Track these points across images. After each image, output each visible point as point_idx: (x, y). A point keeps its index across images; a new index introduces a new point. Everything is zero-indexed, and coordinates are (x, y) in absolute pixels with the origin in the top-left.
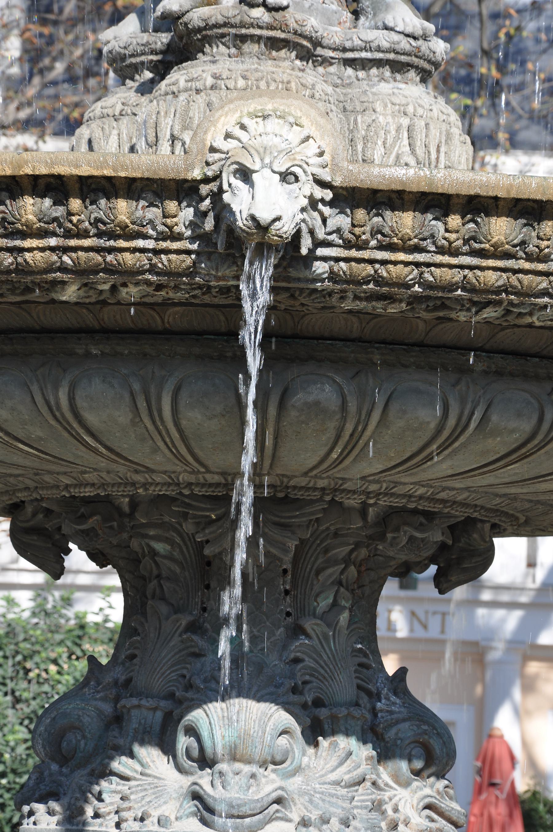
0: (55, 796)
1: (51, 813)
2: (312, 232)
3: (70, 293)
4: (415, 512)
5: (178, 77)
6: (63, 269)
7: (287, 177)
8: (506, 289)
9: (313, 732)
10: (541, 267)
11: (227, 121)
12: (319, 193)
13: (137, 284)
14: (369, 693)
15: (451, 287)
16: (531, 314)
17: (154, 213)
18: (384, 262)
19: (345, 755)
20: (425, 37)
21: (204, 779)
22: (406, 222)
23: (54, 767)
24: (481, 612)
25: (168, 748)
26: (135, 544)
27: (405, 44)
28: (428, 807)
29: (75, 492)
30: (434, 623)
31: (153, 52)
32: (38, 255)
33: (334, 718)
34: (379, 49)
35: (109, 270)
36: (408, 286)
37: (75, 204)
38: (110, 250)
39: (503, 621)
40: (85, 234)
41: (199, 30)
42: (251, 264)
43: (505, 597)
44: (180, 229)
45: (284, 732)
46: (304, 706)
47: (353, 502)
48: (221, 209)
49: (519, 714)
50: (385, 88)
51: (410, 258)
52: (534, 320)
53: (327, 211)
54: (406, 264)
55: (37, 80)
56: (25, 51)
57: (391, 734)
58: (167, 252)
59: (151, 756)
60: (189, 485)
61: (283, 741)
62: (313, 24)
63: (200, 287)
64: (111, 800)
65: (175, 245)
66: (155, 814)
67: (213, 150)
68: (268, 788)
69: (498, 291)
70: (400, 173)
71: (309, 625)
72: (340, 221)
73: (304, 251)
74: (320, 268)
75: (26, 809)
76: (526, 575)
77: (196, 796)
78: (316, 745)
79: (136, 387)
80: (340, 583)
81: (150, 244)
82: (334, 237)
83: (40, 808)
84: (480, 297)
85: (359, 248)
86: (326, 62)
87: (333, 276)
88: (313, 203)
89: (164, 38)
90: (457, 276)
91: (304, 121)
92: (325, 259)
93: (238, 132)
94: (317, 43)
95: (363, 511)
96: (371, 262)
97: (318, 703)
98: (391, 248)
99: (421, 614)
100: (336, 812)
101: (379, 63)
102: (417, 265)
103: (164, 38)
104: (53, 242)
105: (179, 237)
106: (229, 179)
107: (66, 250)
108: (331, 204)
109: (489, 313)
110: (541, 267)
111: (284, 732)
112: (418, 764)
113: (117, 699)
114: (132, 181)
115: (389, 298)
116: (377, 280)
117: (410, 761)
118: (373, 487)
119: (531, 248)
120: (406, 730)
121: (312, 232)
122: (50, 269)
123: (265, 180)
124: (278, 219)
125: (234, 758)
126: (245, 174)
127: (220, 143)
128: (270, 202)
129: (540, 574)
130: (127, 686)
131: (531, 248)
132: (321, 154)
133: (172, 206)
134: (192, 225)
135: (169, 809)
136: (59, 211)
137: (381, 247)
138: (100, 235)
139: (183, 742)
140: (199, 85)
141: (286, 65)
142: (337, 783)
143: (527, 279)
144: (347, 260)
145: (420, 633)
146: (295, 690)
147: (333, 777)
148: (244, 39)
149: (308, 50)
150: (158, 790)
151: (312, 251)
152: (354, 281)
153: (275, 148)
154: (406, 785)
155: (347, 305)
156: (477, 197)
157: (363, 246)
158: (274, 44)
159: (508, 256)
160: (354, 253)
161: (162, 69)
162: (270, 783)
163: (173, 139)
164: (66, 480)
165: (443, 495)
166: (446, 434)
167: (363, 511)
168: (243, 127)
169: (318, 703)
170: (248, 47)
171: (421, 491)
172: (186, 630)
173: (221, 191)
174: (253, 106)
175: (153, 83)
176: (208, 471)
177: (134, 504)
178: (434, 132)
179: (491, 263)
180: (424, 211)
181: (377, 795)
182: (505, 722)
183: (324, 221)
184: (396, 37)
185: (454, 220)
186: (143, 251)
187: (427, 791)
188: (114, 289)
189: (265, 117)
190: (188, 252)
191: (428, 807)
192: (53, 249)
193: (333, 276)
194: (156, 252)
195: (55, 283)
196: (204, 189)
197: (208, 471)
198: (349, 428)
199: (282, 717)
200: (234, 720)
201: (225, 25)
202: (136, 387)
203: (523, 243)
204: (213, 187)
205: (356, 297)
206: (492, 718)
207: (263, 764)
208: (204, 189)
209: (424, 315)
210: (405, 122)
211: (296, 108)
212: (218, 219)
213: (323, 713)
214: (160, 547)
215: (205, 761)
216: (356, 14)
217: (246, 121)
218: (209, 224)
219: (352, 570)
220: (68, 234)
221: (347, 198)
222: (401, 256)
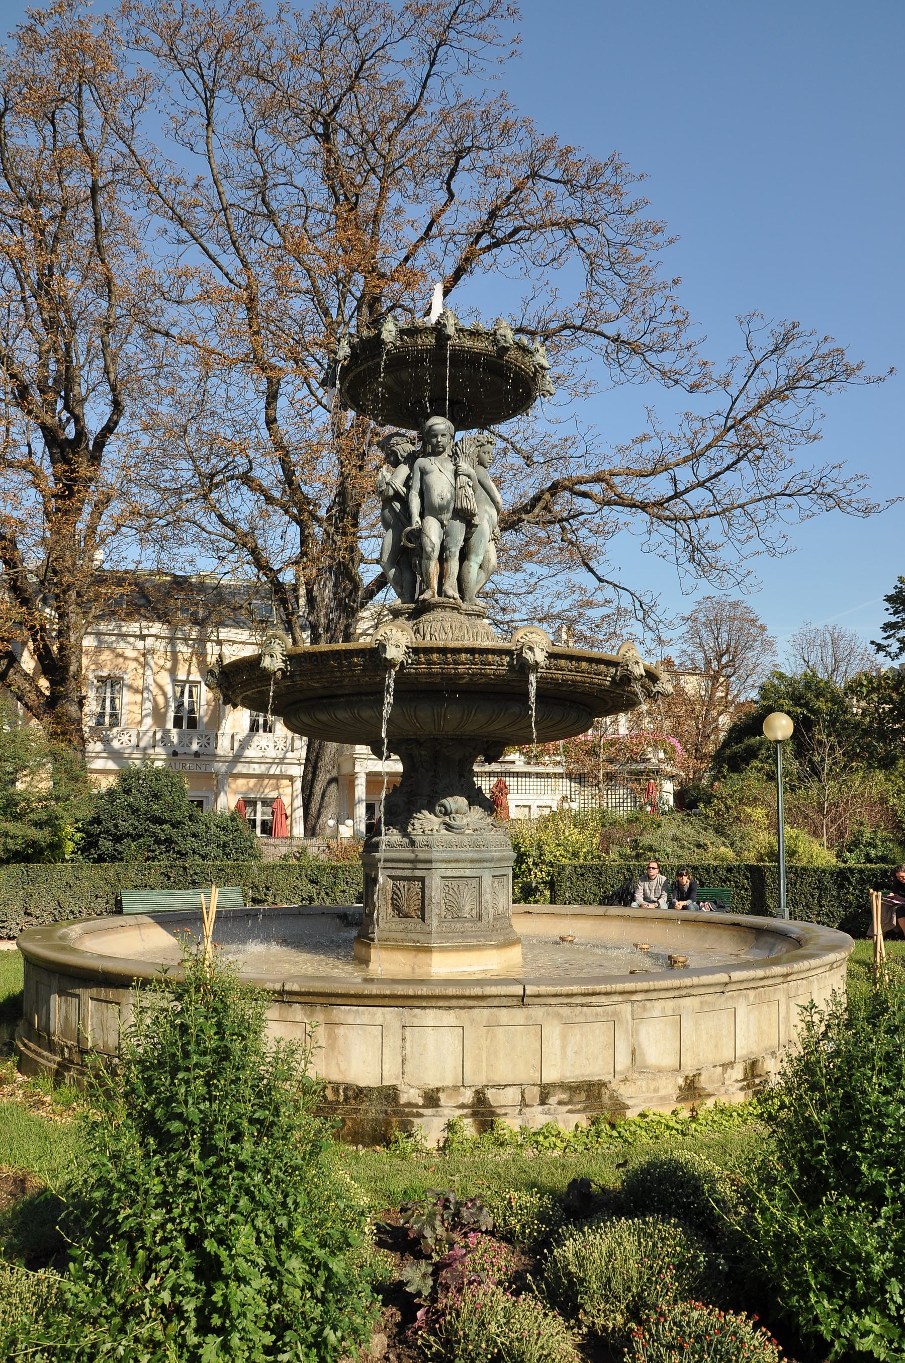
22: (563, 662)
64: (417, 826)
125: (456, 813)
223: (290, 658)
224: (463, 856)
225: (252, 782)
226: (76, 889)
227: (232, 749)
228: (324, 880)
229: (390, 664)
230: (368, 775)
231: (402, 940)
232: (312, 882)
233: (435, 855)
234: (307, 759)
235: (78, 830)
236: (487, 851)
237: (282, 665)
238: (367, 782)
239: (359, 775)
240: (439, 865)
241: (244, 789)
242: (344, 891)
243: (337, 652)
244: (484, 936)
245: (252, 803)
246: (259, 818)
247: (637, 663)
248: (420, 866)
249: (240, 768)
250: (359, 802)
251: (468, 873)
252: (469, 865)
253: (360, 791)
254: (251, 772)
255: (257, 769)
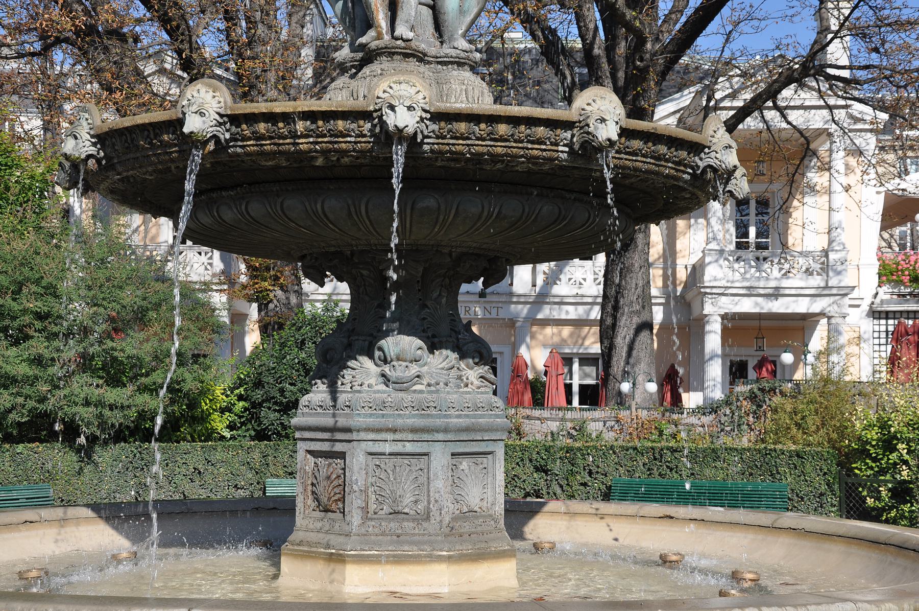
0: (325, 377)
1: (324, 383)
2: (422, 132)
3: (320, 162)
4: (472, 254)
5: (366, 70)
6: (316, 151)
7: (410, 108)
8: (506, 155)
9: (432, 348)
10: (520, 145)
11: (384, 85)
12: (424, 115)
13: (348, 157)
14: (455, 332)
15: (483, 154)
16: (517, 166)
17: (354, 126)
18: (453, 145)
19: (445, 358)
20: (471, 52)
21: (387, 369)
22: (462, 127)
23: (324, 365)
24: (513, 306)
25: (371, 357)
26: (354, 271)
27: (463, 55)
28: (481, 377)
29: (327, 249)
30: (494, 312)
31: (356, 61)
32: (306, 146)
33: (441, 342)
34: (452, 57)
35: (336, 151)
36: (464, 154)
37: (320, 123)
38: (336, 142)
39: (522, 309)
40: (325, 136)
41: (375, 50)
42: (397, 146)
43: (522, 300)
44: (366, 132)
45: (420, 348)
46: (428, 337)
47: (446, 251)
48: (383, 123)
49: (528, 347)
50: (455, 73)
51: (465, 142)
52: (519, 168)
53: (428, 122)
54: (463, 145)
55: (318, 86)
56: (314, 74)
57: (465, 348)
58: (360, 142)
59: (365, 361)
60: (376, 245)
61: (419, 352)
62: (423, 46)
63: (375, 157)
64: (348, 378)
65: (363, 140)
66: (367, 383)
67: (378, 98)
68: (413, 372)
69: (503, 155)
70: (458, 105)
71: (429, 303)
72: (435, 127)
73: (419, 140)
74: (426, 147)
75: (313, 382)
76: (531, 290)
77: (383, 375)
78: (434, 354)
79: (350, 202)
80: (442, 286)
81: (353, 139)
82: (431, 134)
83: (319, 381)
84: (495, 158)
85: (443, 139)
86: (429, 63)
87: (432, 151)
88: (422, 119)
89: (360, 55)
90: (485, 150)
91: (417, 84)
92: (428, 144)
93: (389, 90)
94: (425, 55)
95: (450, 254)
96: (448, 144)
97: (434, 336)
98: (457, 138)
99: (488, 307)
100: (442, 381)
101: (452, 63)
102: (468, 145)
103: (360, 55)
104: (311, 140)
105: (365, 136)
106: (385, 110)
107: (317, 143)
108: (430, 120)
109: (499, 166)
110: (520, 145)
111: (420, 348)
112: (477, 360)
113: (349, 337)
114: (343, 112)
115: (456, 160)
116: (450, 152)
117: (473, 358)
118: (454, 244)
119: (516, 137)
120: (472, 346)
121: (422, 132)
122: (310, 151)
123: (401, 110)
124: (407, 126)
125: (398, 359)
126: (392, 108)
127: (381, 95)
128: (403, 119)
129: (538, 289)
130: (352, 332)
131: (516, 137)
132: (425, 98)
133: (361, 122)
134: (370, 130)
135: (372, 381)
136: (313, 127)
137: (452, 138)
138: (331, 136)
139: (377, 354)
140: (375, 73)
141: (413, 64)
142: (443, 369)
143: (514, 150)
144: (437, 144)
145: (488, 316)
146: (424, 331)
147: (441, 366)
148: (394, 53)
149: (421, 58)
150: (368, 374)
151: (422, 140)
152: (441, 152)
153: (404, 99)
154: (472, 369)
155: (439, 164)
156: (492, 115)
157: (444, 137)
158: (406, 56)
159: (506, 140)
160: (440, 141)
161: (360, 68)
162: (414, 369)
163: (365, 96)
164: (323, 244)
165: (484, 246)
166: (483, 219)
167: (450, 254)
168: (391, 88)
169: (434, 336)
170: (395, 57)
171: (475, 245)
172: (377, 307)
173: (382, 115)
174: (395, 78)
175: (356, 74)
176: (383, 238)
177: (352, 254)
178: (476, 91)
179: (499, 144)
180: (470, 122)
181: (459, 373)
182: (523, 351)
183: (427, 127)
184: (459, 52)
185: (483, 126)
186: (350, 142)
187: (481, 371)
188: (338, 159)
189: (400, 83)
190: (369, 142)
191: (481, 377)
192: (311, 143)
193: (432, 151)
194: (356, 143)
195: (313, 157)
196: (375, 115)
197: (383, 238)
198: (441, 217)
199: (419, 342)
200: (399, 343)
201: (386, 48)
202: (350, 202)
203: (512, 135)
204: (379, 113)
205: (442, 160)
206: (519, 349)
207: (411, 362)
208: (375, 115)
209: (471, 167)
210: (464, 87)
211: (413, 79)
212: (381, 128)
213: (436, 340)
214: (365, 272)
215: (385, 361)
216: (442, 43)
217: (392, 85)
218: (378, 130)
219: (447, 280)
220: (318, 136)
221: (437, 117)
222: (461, 142)
223: (102, 138)
224: (400, 422)
225: (566, 331)
226: (208, 478)
227: (534, 285)
228: (557, 467)
229: (191, 141)
230: (724, 317)
231: (317, 544)
232: (537, 469)
233: (358, 421)
234: (605, 296)
235: (240, 398)
236: (439, 417)
237: (92, 150)
238: (725, 330)
239: (712, 319)
240: (363, 435)
241: (556, 339)
242: (585, 485)
243: (143, 127)
244: (430, 543)
245: (568, 361)
246: (576, 383)
247: (603, 120)
248: (339, 436)
249: (545, 313)
250: (711, 358)
251: (409, 448)
252: (410, 437)
253: (713, 341)
254: (563, 317)
255: (572, 313)
